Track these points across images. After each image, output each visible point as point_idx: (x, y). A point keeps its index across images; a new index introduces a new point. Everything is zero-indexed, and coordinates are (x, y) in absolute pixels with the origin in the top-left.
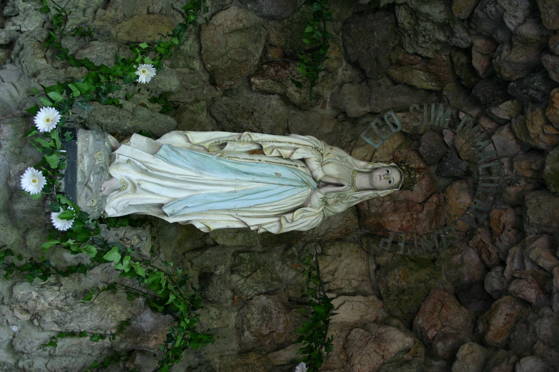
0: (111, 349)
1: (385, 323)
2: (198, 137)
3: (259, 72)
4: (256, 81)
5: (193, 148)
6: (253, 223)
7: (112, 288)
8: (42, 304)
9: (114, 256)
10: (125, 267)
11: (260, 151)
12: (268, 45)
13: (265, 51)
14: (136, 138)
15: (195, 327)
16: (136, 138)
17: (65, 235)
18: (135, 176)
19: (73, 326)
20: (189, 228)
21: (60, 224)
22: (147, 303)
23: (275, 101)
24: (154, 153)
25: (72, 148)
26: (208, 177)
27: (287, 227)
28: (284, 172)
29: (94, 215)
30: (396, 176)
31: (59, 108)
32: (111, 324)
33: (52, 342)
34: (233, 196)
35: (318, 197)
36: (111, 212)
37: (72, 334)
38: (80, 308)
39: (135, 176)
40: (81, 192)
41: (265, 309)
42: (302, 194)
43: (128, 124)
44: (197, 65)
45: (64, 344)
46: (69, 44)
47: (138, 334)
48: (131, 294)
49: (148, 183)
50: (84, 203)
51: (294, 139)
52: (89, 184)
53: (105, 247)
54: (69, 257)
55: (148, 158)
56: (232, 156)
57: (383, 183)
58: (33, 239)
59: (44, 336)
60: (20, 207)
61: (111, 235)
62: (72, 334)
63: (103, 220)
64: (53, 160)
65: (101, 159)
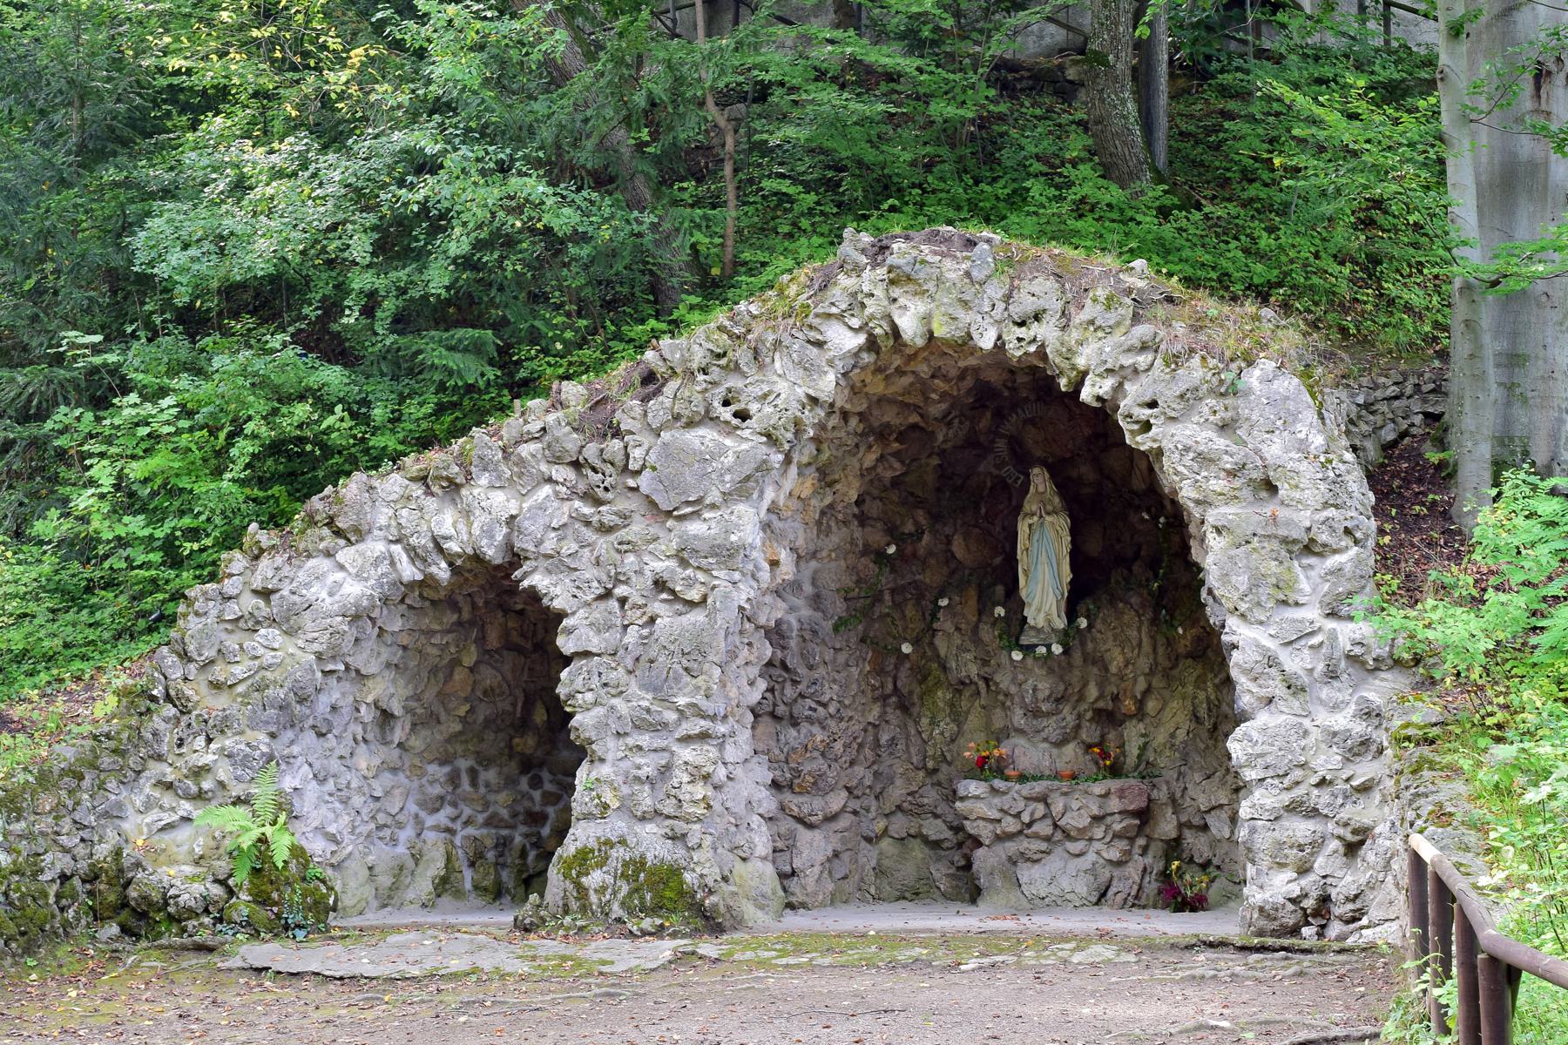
28: (1036, 537)
30: (1036, 471)
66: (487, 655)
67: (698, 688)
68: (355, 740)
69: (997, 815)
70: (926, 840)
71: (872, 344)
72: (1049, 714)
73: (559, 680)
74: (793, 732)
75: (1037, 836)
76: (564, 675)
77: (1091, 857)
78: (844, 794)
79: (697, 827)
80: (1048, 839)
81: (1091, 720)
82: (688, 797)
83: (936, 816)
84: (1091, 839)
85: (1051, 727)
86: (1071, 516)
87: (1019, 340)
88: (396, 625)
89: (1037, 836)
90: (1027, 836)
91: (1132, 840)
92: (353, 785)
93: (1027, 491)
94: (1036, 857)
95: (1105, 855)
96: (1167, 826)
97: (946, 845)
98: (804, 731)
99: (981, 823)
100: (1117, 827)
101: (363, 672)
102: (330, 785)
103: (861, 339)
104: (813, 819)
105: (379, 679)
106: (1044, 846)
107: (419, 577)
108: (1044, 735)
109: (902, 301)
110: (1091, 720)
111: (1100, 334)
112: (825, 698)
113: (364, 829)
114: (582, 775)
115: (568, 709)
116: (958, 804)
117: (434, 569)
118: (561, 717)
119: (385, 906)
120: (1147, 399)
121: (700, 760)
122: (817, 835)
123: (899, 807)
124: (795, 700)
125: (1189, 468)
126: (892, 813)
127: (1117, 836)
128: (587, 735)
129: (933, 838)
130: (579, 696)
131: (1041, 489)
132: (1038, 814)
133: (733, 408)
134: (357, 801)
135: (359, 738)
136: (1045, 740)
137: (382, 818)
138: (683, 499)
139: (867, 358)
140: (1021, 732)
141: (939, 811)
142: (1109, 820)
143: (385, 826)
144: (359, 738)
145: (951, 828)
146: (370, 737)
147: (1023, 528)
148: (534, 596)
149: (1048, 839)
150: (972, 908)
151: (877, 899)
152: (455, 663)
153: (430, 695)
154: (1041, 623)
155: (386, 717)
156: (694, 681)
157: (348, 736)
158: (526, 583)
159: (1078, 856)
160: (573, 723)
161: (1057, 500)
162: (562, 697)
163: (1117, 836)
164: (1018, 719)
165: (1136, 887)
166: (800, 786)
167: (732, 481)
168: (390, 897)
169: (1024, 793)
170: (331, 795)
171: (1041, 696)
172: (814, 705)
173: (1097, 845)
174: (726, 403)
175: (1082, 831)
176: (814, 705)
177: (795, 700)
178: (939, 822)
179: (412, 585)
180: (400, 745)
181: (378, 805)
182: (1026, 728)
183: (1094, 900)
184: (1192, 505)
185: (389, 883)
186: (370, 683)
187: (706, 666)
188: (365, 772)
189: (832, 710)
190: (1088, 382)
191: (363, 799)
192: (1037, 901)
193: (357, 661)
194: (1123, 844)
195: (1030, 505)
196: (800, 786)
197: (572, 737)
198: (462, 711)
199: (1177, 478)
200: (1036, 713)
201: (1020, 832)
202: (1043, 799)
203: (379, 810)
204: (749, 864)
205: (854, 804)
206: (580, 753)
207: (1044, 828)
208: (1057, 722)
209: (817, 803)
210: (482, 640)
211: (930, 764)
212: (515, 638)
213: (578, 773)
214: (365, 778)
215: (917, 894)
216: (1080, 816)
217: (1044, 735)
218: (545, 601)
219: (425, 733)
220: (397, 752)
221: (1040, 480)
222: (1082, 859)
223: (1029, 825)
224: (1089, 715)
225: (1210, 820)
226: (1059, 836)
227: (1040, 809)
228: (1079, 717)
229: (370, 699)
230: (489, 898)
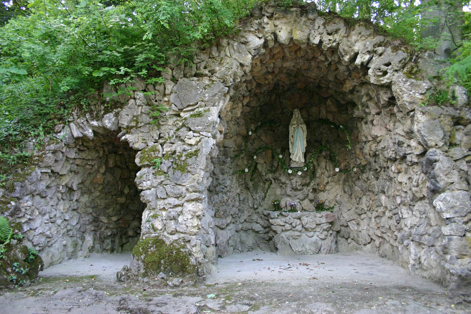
0: (329, 160)
1: (326, 104)
2: (290, 147)
3: (274, 131)
4: (276, 132)
5: (292, 148)
6: (305, 137)
7: (317, 160)
8: (320, 172)
9: (311, 161)
10: (313, 159)
11: (293, 136)
12: (268, 129)
13: (269, 130)
14: (291, 157)
15: (419, 62)
16: (291, 157)
17: (308, 168)
18: (298, 157)
19: (324, 167)
20: (306, 148)
21: (306, 169)
22: (321, 154)
23: (280, 128)
24: (294, 154)
25: (294, 168)
26: (297, 145)
27: (306, 130)
28: (296, 132)
29: (304, 164)
30: (296, 110)
31: (288, 170)
32: (324, 160)
33: (327, 170)
34: (301, 141)
35: (301, 126)
36: (304, 161)
37: (326, 167)
38: (321, 165)
39: (298, 157)
40: (301, 166)
41: (323, 129)
42: (300, 129)
43: (288, 158)
44: (273, 144)
45: (328, 168)
46: (274, 169)
47: (326, 155)
48: (319, 157)
49: (299, 155)
50: (302, 165)
51: (290, 129)
52: (184, 129)
53: (309, 162)
54: (311, 168)
55: (294, 155)
56: (294, 141)
57: (297, 113)
58: (308, 173)
59: (326, 172)
60: (303, 175)
61: (308, 161)
62: (326, 167)
63: (305, 162)
64: (296, 170)
65: (295, 163)
66: (108, 169)
67: (194, 179)
68: (58, 199)
69: (284, 224)
70: (254, 231)
71: (265, 45)
72: (300, 190)
73: (136, 176)
74: (216, 196)
75: (297, 230)
76: (138, 174)
77: (315, 237)
78: (231, 217)
79: (194, 237)
80: (300, 231)
81: (312, 192)
82: (191, 225)
83: (257, 223)
84: (315, 232)
85: (300, 195)
86: (306, 125)
87: (330, 40)
88: (72, 155)
89: (297, 230)
90: (293, 231)
91: (328, 231)
92: (57, 216)
93: (292, 117)
94: (296, 238)
95: (320, 237)
96: (337, 228)
97: (260, 232)
98: (220, 196)
99: (278, 226)
100: (325, 227)
101: (60, 173)
102: (47, 217)
103: (262, 41)
104: (223, 226)
105: (67, 176)
106: (299, 234)
107: (81, 135)
108: (298, 197)
109: (280, 26)
110: (312, 192)
111: (363, 38)
112: (226, 185)
113: (62, 232)
114: (146, 215)
115: (140, 188)
116: (270, 220)
117: (86, 132)
118: (137, 192)
119: (71, 259)
120: (386, 62)
121: (195, 209)
122: (224, 232)
123: (245, 220)
124: (217, 186)
125: (407, 89)
126: (243, 222)
127: (324, 230)
128: (148, 198)
129: (257, 230)
130: (145, 183)
131: (297, 116)
132: (298, 223)
133: (209, 69)
134: (59, 221)
135: (60, 198)
136: (298, 199)
137: (69, 227)
138: (188, 104)
139: (263, 51)
140: (289, 196)
141: (258, 222)
142: (322, 225)
143: (70, 230)
144: (60, 198)
145: (263, 227)
146: (64, 198)
147: (291, 129)
148: (126, 143)
149: (300, 231)
150: (274, 255)
151: (242, 251)
152: (98, 171)
153: (88, 182)
154: (297, 160)
155: (71, 190)
156: (193, 176)
157: (55, 199)
158: (123, 138)
159: (311, 237)
160: (142, 193)
161: (302, 120)
162: (137, 183)
163: (324, 230)
164: (289, 191)
165: (329, 247)
166: (218, 215)
167: (209, 96)
168: (72, 255)
169: (294, 216)
170: (47, 220)
171: (298, 184)
172: (224, 187)
173: (317, 233)
174: (205, 68)
175: (313, 229)
176: (224, 187)
177: (217, 186)
178: (258, 225)
179: (78, 139)
180: (77, 200)
181: (67, 222)
182: (291, 195)
183: (317, 252)
184: (407, 104)
185: (72, 251)
186: (64, 178)
187: (198, 170)
188: (62, 211)
189: (228, 189)
190: (359, 57)
191: (61, 221)
192: (298, 253)
193: (57, 168)
194: (325, 233)
195: (294, 121)
196: (218, 215)
197: (141, 199)
198: (100, 188)
199: (401, 93)
200: (296, 189)
201: (291, 229)
202: (299, 219)
203: (68, 224)
204: (210, 248)
205: (233, 221)
206: (143, 206)
207: (299, 228)
208: (302, 193)
209: (224, 221)
210: (106, 163)
211: (255, 206)
212: (119, 164)
213: (143, 214)
214: (62, 213)
215: (252, 249)
216: (313, 224)
217: (298, 197)
218: (131, 145)
219: (86, 196)
220: (75, 203)
221: (297, 113)
222: (312, 238)
223: (294, 227)
224: (311, 190)
225: (349, 224)
226: (304, 230)
227: (298, 222)
228: (309, 190)
229: (63, 184)
230: (109, 252)
